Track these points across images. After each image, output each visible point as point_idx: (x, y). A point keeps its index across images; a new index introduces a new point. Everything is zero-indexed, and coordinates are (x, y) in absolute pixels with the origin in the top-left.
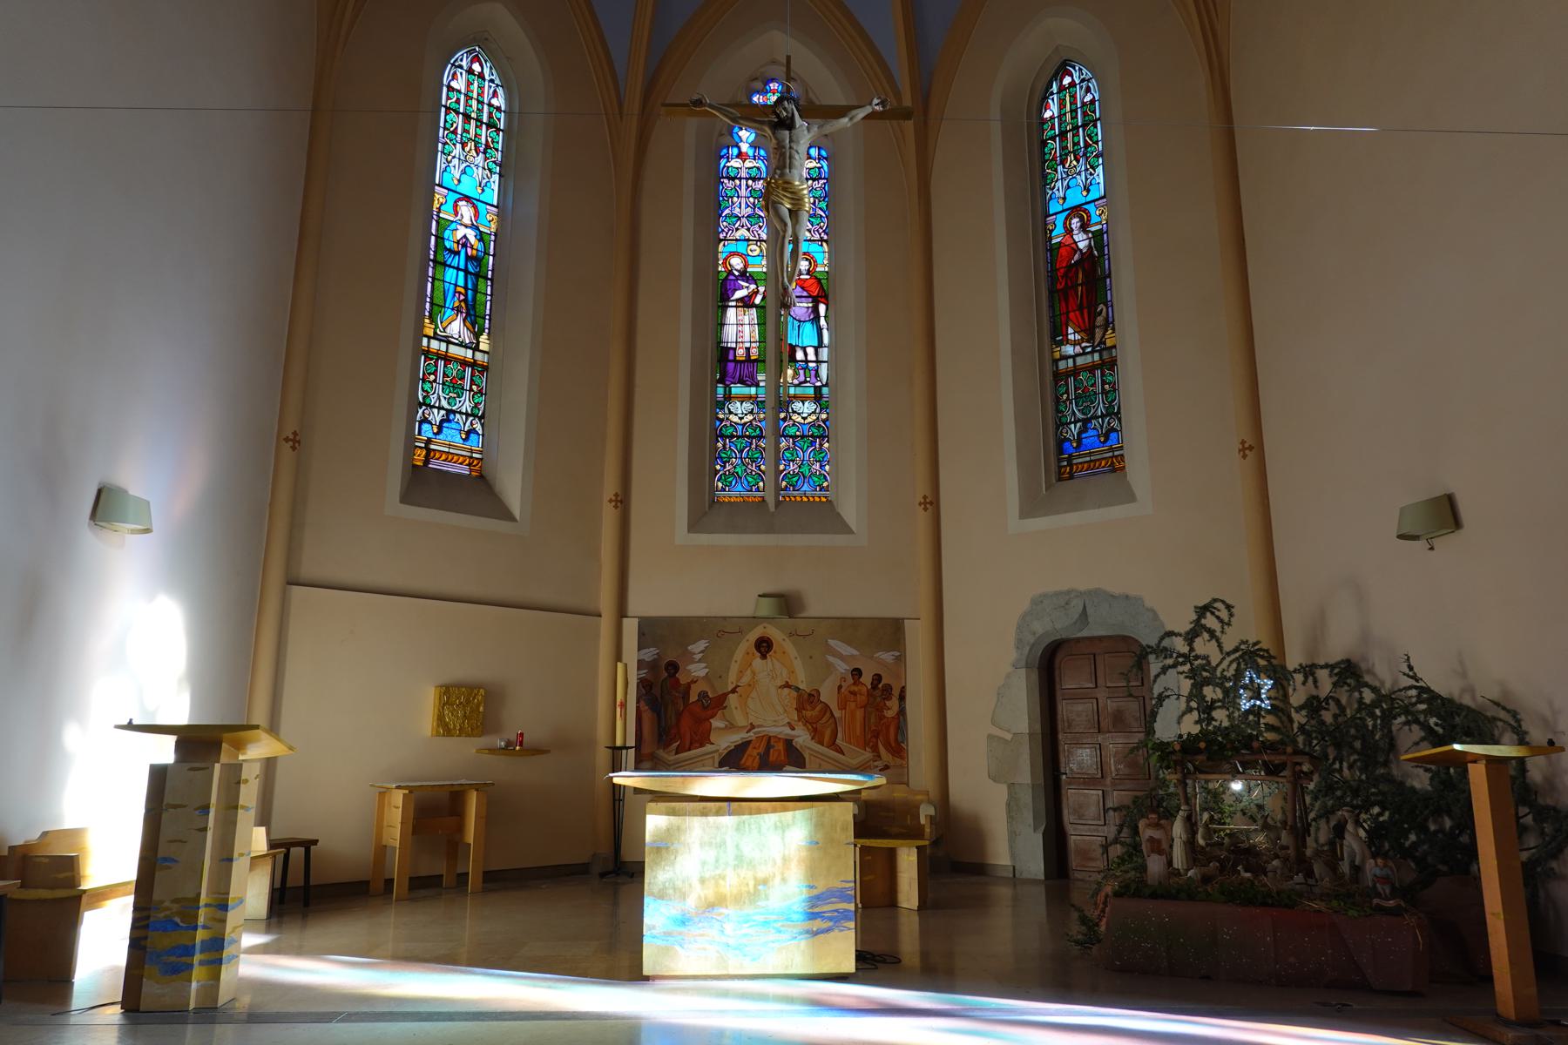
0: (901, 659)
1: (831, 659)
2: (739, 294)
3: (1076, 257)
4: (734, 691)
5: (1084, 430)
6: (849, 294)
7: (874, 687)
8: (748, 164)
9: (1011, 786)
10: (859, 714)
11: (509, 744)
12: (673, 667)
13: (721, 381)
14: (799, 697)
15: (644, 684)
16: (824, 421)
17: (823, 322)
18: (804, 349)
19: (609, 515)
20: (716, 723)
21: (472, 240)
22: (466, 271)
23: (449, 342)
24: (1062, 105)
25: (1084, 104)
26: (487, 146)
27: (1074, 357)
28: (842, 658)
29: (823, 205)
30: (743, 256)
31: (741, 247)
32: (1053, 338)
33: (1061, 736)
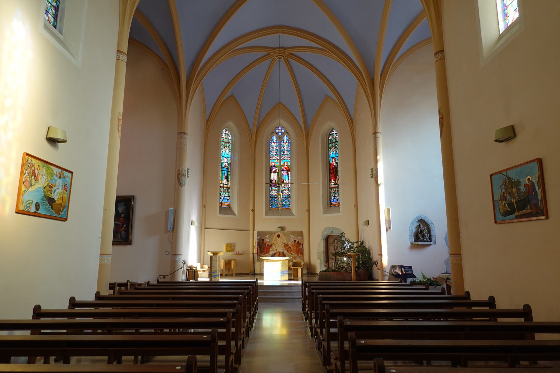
0: (303, 238)
1: (290, 238)
2: (274, 170)
3: (334, 167)
4: (273, 244)
5: (334, 198)
6: (294, 170)
7: (298, 243)
8: (275, 144)
9: (320, 260)
10: (295, 248)
11: (236, 253)
12: (263, 240)
13: (271, 187)
14: (285, 245)
15: (258, 243)
16: (290, 194)
17: (289, 175)
18: (286, 180)
19: (251, 213)
20: (270, 249)
21: (227, 165)
22: (226, 171)
23: (224, 184)
24: (332, 137)
25: (336, 138)
26: (229, 147)
27: (333, 185)
28: (292, 238)
29: (289, 152)
30: (274, 163)
31: (274, 161)
32: (330, 181)
33: (329, 251)
